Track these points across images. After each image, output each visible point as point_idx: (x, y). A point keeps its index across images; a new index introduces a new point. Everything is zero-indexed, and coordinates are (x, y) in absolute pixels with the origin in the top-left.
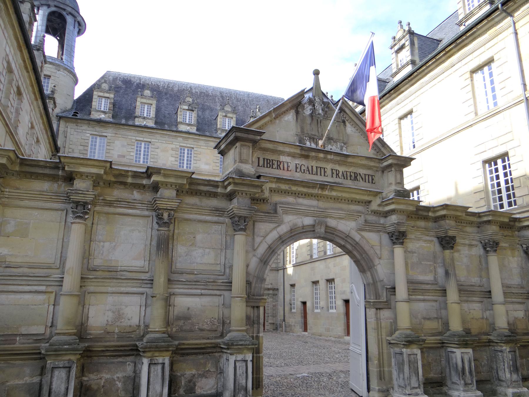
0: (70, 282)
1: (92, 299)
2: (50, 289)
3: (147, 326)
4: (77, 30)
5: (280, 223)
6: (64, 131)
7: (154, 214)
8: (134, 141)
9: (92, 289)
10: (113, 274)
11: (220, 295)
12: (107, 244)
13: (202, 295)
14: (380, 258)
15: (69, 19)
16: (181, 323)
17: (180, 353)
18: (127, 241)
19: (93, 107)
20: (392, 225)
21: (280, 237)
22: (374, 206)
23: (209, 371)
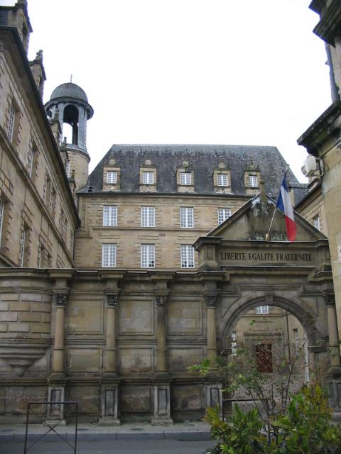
0: (110, 343)
1: (123, 352)
2: (100, 347)
3: (156, 368)
4: (86, 116)
5: (240, 297)
6: (83, 206)
7: (154, 298)
8: (140, 207)
9: (122, 346)
10: (133, 338)
11: (200, 348)
12: (128, 319)
13: (188, 348)
14: (318, 316)
15: (81, 110)
16: (176, 366)
17: (175, 384)
18: (141, 316)
19: (104, 181)
20: (324, 291)
21: (240, 307)
22: (310, 278)
23: (196, 396)
